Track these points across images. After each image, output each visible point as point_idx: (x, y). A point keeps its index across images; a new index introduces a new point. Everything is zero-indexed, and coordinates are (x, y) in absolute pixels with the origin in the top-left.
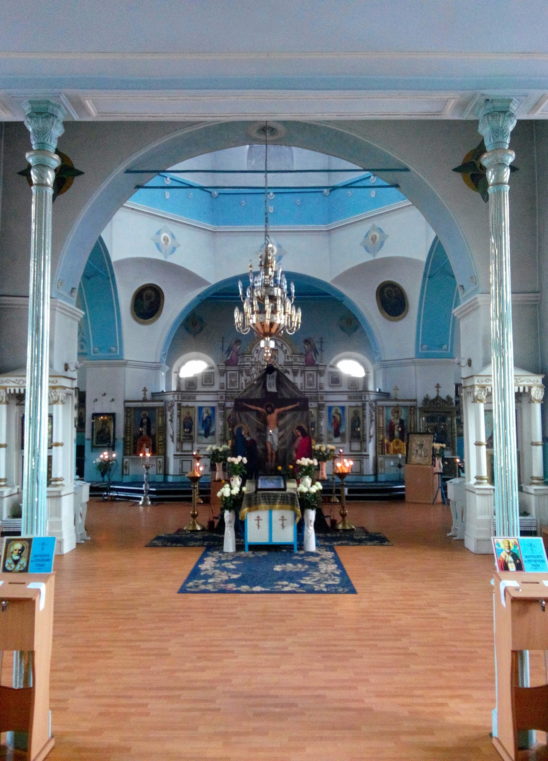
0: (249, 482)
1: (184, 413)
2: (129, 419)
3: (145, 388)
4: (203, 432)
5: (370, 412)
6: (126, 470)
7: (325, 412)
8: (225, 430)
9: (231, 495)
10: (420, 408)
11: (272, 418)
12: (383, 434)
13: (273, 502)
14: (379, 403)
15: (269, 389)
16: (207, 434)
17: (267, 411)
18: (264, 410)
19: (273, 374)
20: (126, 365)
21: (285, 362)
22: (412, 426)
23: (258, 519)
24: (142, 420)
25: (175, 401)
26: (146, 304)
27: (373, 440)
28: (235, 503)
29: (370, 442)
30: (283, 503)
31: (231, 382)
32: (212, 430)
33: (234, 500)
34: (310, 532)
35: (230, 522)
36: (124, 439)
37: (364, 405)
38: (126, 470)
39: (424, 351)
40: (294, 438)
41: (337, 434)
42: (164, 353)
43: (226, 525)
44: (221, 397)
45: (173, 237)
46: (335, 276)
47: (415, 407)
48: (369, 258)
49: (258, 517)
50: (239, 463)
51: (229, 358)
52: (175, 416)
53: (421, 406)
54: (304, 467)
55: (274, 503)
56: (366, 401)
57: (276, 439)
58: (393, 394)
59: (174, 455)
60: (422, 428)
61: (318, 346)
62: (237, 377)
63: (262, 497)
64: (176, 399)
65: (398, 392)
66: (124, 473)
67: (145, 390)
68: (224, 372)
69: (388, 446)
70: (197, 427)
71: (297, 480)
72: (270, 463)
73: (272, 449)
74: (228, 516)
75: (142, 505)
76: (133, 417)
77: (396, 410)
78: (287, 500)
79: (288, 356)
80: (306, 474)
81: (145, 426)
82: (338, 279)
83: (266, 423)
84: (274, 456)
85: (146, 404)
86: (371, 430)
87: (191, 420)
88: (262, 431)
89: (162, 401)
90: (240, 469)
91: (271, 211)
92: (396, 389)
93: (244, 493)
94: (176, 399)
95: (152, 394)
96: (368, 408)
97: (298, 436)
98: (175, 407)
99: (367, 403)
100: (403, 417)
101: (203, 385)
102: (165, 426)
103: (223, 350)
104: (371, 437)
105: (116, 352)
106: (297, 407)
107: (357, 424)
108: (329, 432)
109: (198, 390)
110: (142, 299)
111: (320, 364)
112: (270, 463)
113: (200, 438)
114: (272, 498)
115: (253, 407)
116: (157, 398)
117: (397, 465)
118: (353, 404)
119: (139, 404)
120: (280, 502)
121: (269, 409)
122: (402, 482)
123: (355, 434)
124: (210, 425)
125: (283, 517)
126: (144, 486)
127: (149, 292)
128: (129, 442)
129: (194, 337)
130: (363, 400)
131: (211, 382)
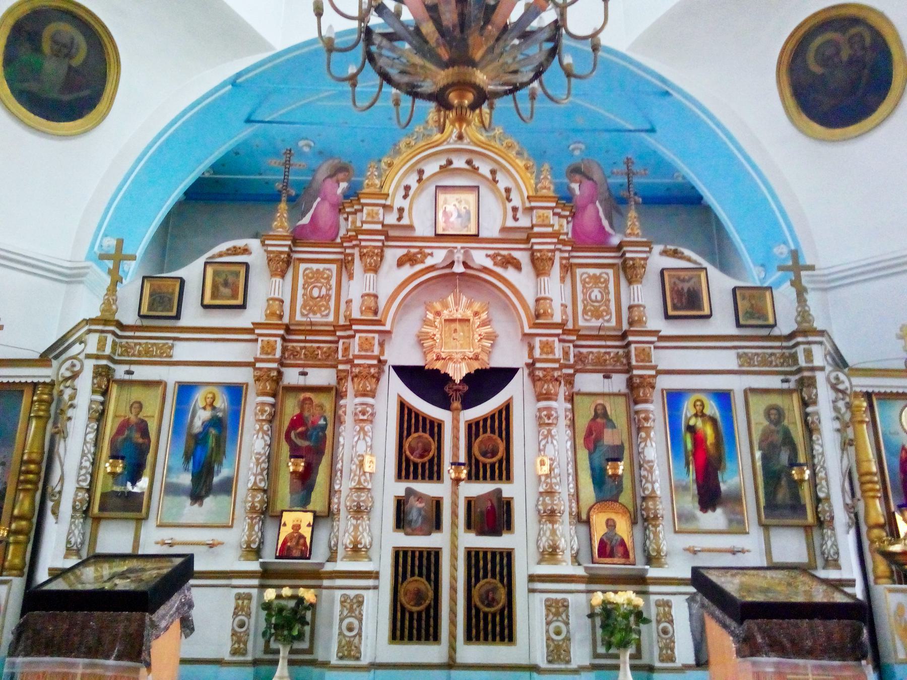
1: (118, 405)
4: (186, 479)
5: (836, 409)
7: (655, 409)
8: (271, 469)
21: (504, 229)
25: (88, 356)
26: (53, 69)
31: (309, 298)
32: (223, 473)
41: (709, 496)
44: (268, 349)
56: (813, 369)
62: (333, 282)
64: (92, 348)
68: (288, 263)
70: (167, 462)
79: (515, 209)
87: (145, 432)
108: (677, 489)
109: (184, 322)
110: (37, 49)
113: (171, 502)
124: (220, 449)
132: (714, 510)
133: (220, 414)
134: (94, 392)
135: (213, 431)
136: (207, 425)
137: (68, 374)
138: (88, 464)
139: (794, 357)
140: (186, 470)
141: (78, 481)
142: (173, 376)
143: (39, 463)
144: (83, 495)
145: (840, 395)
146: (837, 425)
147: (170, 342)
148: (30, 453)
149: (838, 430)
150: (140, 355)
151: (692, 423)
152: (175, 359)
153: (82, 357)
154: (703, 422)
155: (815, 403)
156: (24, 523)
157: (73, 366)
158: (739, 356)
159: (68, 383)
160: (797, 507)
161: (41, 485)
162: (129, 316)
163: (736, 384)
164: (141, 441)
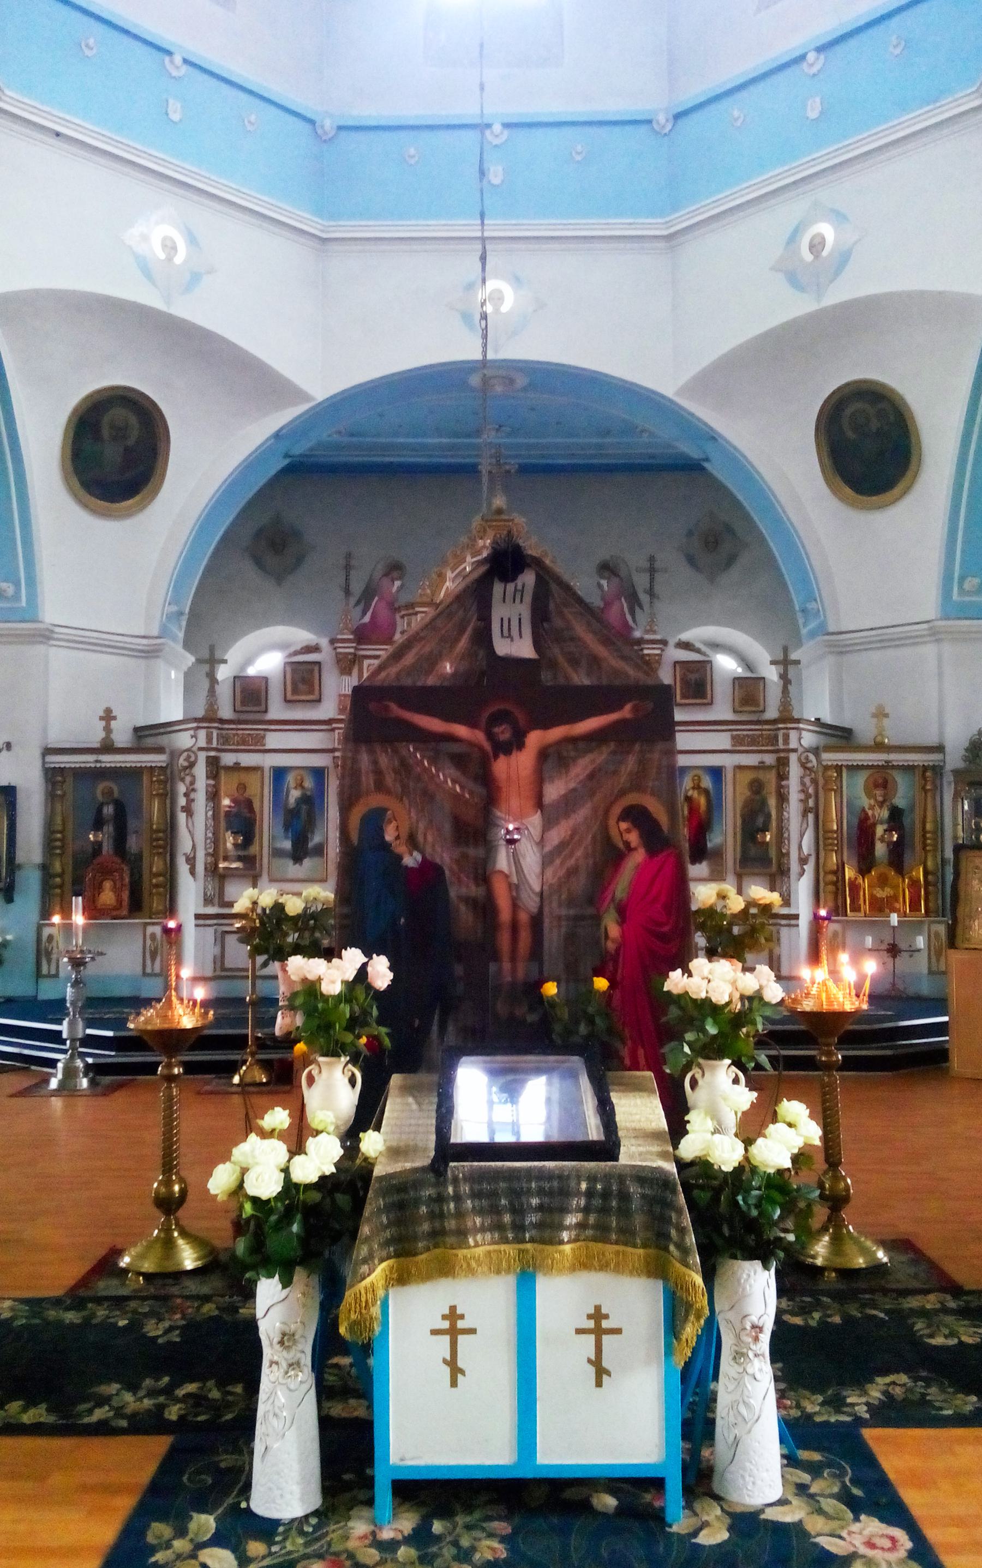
0: (406, 1090)
2: (58, 807)
3: (108, 711)
4: (287, 845)
5: (803, 784)
6: (49, 961)
9: (290, 1187)
10: (956, 772)
11: (516, 768)
12: (839, 852)
13: (540, 1226)
14: (830, 758)
15: (502, 648)
16: (298, 855)
17: (490, 736)
18: (479, 736)
19: (519, 582)
20: (49, 638)
22: (929, 826)
23: (453, 1327)
24: (99, 811)
25: (201, 749)
26: (112, 453)
27: (809, 868)
28: (316, 1230)
29: (802, 873)
30: (602, 1233)
32: (316, 839)
33: (310, 1212)
34: (753, 1399)
35: (286, 1340)
36: (45, 868)
37: (783, 763)
38: (49, 961)
39: (967, 599)
40: (613, 856)
42: (174, 608)
43: (269, 1352)
45: (192, 240)
46: (681, 382)
47: (937, 770)
48: (800, 306)
49: (453, 1315)
50: (350, 986)
51: (367, 619)
52: (200, 797)
53: (960, 764)
54: (708, 1008)
55: (548, 1233)
57: (531, 859)
58: (865, 730)
59: (198, 917)
60: (960, 834)
61: (641, 581)
63: (475, 1195)
64: (202, 743)
65: (886, 722)
66: (45, 970)
67: (108, 716)
68: (353, 662)
69: (855, 887)
70: (271, 832)
71: (662, 1079)
72: (507, 966)
73: (515, 905)
74: (277, 1307)
75: (56, 1093)
76: (70, 797)
77: (881, 779)
78: (624, 1212)
80: (713, 1050)
81: (109, 829)
82: (704, 383)
83: (490, 794)
84: (525, 937)
85: (109, 760)
86: (801, 839)
88: (474, 831)
89: (160, 750)
90: (354, 1024)
91: (496, 181)
92: (881, 714)
93: (369, 1165)
94: (202, 743)
95: (137, 730)
96: (795, 771)
97: (629, 848)
98: (200, 770)
99: (793, 757)
100: (900, 801)
101: (286, 701)
102: (170, 828)
103: (347, 592)
104: (803, 861)
105: (17, 597)
106: (623, 722)
107: (760, 821)
110: (97, 437)
111: (647, 637)
112: (507, 966)
114: (535, 1201)
115: (434, 724)
116: (150, 742)
117: (885, 946)
118: (750, 760)
119: (88, 760)
120: (581, 1226)
121: (504, 733)
122: (938, 1004)
123: (753, 851)
125: (598, 1315)
126: (65, 1023)
127: (119, 414)
128: (61, 875)
129: (279, 584)
130: (781, 746)
131: (311, 692)
132: (700, 862)
133: (309, 793)
134: (208, 778)
135: (304, 807)
136: (300, 801)
137: (186, 764)
138: (210, 835)
139: (776, 737)
140: (286, 838)
141: (206, 849)
142: (270, 761)
143: (164, 831)
144: (210, 859)
145: (808, 772)
146: (802, 796)
147: (262, 732)
148: (158, 823)
149: (801, 801)
150: (238, 744)
151: (690, 793)
152: (267, 747)
153: (195, 749)
154: (699, 794)
155: (787, 778)
156: (161, 879)
157: (189, 757)
158: (733, 738)
159: (187, 771)
160: (764, 860)
161: (169, 848)
162: (226, 712)
163: (727, 761)
164: (248, 815)
